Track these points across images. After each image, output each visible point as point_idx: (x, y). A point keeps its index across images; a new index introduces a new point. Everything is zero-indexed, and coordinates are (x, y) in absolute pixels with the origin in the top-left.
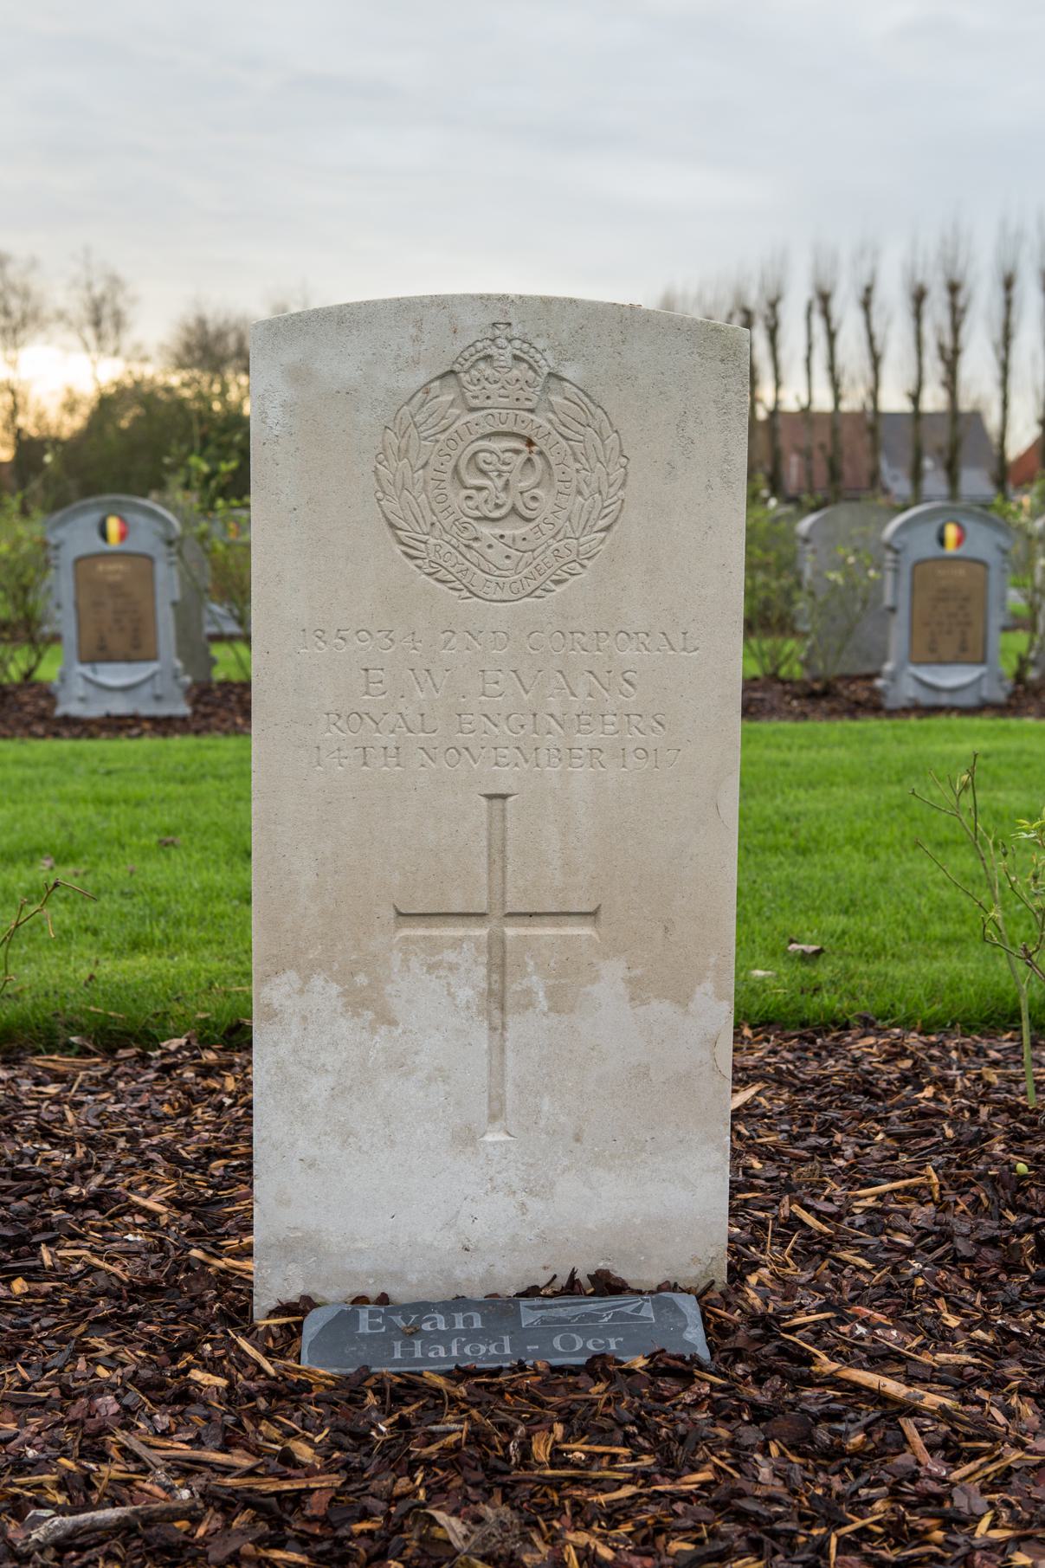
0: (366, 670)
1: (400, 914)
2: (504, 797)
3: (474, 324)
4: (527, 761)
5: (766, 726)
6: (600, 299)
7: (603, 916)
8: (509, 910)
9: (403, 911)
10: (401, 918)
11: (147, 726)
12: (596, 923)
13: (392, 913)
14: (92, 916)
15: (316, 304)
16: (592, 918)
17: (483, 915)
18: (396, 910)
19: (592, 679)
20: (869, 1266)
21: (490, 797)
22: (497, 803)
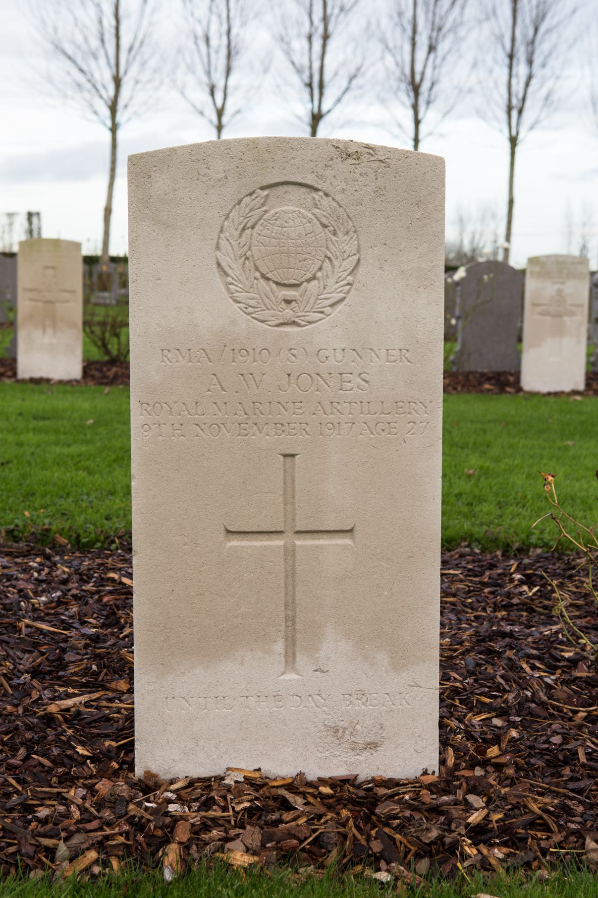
0: (341, 374)
1: (228, 532)
2: (293, 456)
3: (88, 340)
4: (183, 358)
5: (454, 398)
6: (166, 147)
7: (358, 533)
8: (298, 529)
9: (232, 530)
10: (230, 534)
11: (530, 49)
12: (352, 538)
13: (224, 533)
14: (28, 482)
15: (132, 480)
16: (349, 534)
17: (282, 532)
18: (225, 527)
19: (355, 354)
20: (461, 679)
21: (285, 456)
22: (288, 459)
